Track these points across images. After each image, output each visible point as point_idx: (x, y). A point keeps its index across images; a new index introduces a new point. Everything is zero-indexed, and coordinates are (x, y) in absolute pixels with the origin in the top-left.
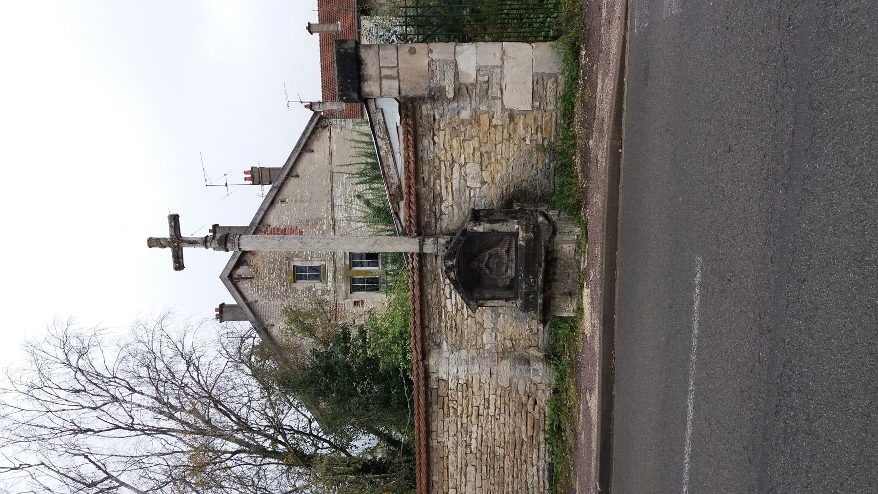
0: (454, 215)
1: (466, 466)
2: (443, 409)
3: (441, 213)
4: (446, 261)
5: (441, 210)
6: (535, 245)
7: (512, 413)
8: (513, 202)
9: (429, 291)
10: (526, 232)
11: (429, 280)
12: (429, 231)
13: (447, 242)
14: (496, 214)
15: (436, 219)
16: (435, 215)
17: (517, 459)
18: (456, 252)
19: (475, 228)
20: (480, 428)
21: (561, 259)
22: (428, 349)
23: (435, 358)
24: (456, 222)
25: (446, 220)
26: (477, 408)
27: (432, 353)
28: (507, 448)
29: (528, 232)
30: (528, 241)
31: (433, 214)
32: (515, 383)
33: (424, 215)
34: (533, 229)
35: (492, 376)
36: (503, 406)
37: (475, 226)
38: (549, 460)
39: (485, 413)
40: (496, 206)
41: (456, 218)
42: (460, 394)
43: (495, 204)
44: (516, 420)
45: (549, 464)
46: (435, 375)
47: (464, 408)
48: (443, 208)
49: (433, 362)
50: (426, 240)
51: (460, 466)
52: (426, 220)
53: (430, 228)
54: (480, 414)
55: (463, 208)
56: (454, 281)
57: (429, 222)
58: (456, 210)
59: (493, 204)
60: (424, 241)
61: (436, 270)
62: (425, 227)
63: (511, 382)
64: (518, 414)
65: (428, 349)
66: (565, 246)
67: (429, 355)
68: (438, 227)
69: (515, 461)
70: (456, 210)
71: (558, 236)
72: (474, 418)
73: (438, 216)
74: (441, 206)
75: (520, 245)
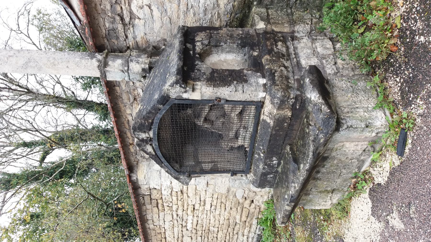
0: (153, 21)
1: (183, 237)
2: (157, 207)
3: (132, 16)
4: (136, 133)
5: (131, 12)
6: (289, 125)
7: (228, 209)
8: (252, 3)
9: (128, 111)
10: (280, 107)
11: (126, 101)
12: (116, 43)
13: (144, 70)
14: (225, 46)
15: (124, 25)
16: (122, 19)
17: (229, 233)
18: (152, 123)
19: (185, 96)
20: (195, 217)
21: (334, 158)
22: (135, 163)
23: (145, 171)
24: (159, 31)
25: (142, 28)
26: (193, 206)
27: (140, 165)
28: (221, 228)
29: (283, 109)
30: (279, 122)
31: (118, 18)
32: (233, 192)
33: (104, 19)
34: (294, 105)
35: (209, 186)
36: (219, 205)
37: (186, 92)
38: (258, 232)
39: (201, 209)
40: (223, 9)
41: (157, 25)
42: (175, 198)
43: (222, 6)
44: (231, 213)
45: (258, 235)
46: (147, 186)
47: (179, 207)
48: (134, 9)
49: (143, 176)
50: (110, 63)
51: (177, 237)
52: (107, 25)
53: (117, 38)
54: (196, 208)
55: (168, 10)
56: (153, 155)
57: (114, 30)
58: (156, 13)
59: (218, 5)
60: (106, 64)
61: (134, 90)
62: (108, 36)
63: (228, 191)
64: (234, 209)
65: (135, 163)
66: (347, 145)
67: (137, 167)
68: (130, 36)
69: (228, 234)
70: (156, 13)
71: (342, 133)
72: (189, 212)
73: (127, 20)
74: (129, 5)
75: (264, 121)
